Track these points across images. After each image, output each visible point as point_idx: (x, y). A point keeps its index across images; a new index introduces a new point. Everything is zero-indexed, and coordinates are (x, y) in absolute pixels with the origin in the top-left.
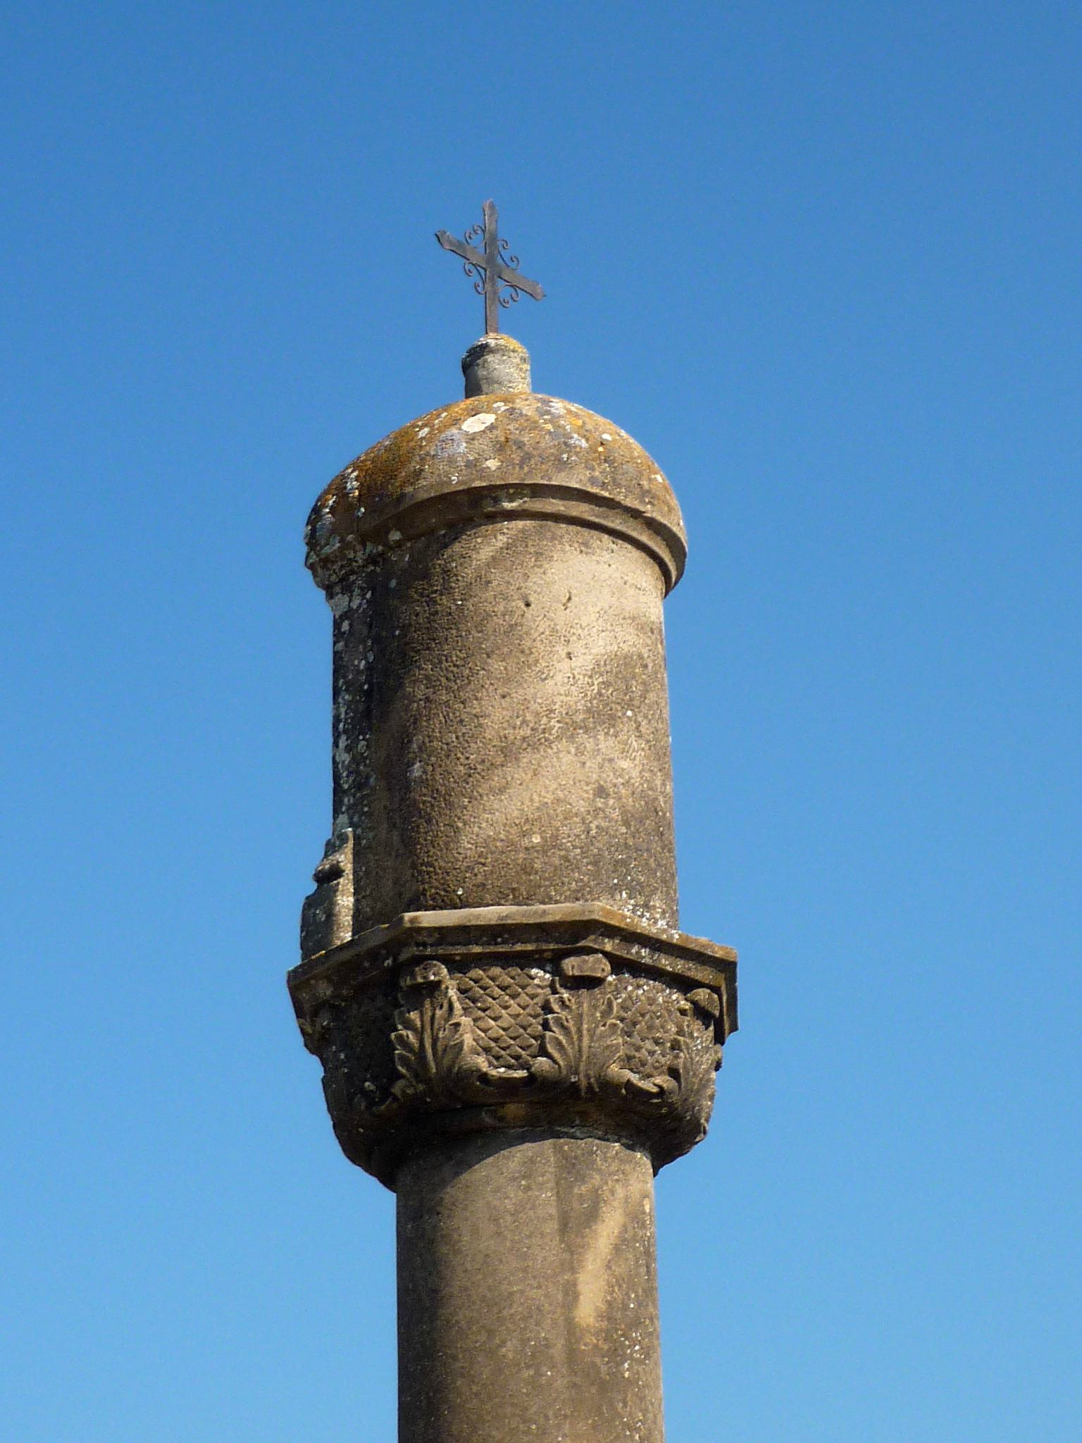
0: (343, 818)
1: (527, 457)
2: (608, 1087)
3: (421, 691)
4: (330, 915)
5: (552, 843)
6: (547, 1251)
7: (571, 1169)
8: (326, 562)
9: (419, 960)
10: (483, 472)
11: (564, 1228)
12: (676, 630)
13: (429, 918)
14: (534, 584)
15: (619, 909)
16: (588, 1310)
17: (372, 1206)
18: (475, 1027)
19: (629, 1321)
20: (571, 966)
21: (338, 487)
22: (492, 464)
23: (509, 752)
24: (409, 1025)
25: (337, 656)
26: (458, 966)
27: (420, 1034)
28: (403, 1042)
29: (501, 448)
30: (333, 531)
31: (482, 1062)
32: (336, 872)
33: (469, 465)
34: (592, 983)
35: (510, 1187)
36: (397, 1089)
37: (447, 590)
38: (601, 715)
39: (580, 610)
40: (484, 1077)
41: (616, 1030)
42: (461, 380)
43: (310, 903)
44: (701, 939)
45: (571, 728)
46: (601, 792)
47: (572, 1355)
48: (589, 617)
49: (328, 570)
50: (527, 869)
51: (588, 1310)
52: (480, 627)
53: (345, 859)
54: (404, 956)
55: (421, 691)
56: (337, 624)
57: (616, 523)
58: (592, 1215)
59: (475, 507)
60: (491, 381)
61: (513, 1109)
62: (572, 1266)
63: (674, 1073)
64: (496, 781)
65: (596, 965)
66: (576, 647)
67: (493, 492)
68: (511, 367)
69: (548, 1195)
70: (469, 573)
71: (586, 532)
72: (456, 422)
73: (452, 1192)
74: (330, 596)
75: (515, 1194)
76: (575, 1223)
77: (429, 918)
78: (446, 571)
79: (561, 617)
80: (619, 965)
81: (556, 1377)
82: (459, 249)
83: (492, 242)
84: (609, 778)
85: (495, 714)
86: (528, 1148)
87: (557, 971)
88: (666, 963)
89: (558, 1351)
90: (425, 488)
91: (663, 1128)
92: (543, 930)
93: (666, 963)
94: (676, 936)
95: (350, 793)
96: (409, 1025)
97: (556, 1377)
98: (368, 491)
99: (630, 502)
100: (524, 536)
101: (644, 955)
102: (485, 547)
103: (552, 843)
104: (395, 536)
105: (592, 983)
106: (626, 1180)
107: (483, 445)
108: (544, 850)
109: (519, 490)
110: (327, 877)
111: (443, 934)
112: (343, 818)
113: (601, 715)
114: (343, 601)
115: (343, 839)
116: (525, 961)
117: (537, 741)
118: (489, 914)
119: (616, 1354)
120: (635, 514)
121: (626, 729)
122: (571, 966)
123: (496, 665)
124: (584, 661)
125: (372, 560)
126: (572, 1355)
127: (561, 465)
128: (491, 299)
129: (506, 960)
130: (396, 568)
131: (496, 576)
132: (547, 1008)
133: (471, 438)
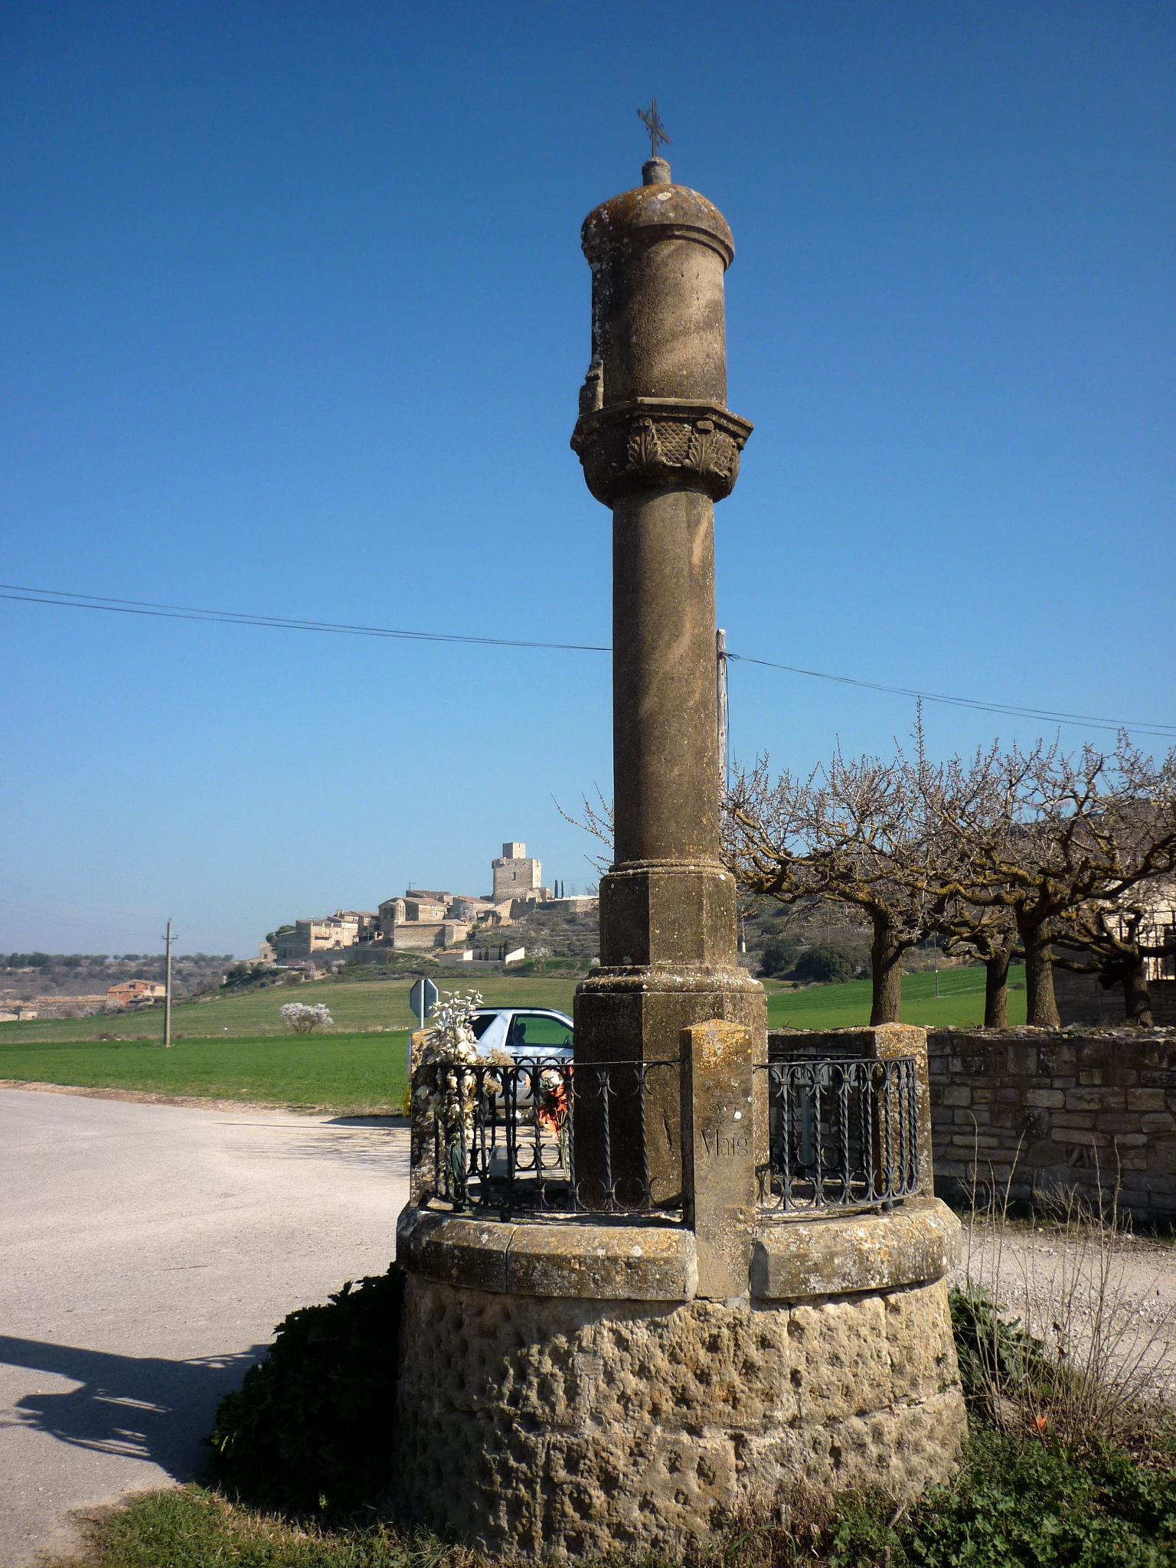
0: (597, 356)
1: (685, 214)
2: (709, 472)
3: (636, 307)
4: (594, 395)
5: (690, 375)
6: (682, 534)
7: (692, 504)
8: (592, 248)
9: (640, 417)
10: (668, 218)
11: (689, 527)
12: (729, 289)
13: (648, 400)
14: (686, 266)
15: (713, 402)
16: (696, 559)
17: (603, 516)
18: (663, 445)
19: (707, 563)
20: (700, 424)
21: (596, 215)
22: (672, 215)
23: (674, 336)
24: (635, 442)
25: (594, 289)
26: (656, 420)
27: (640, 446)
28: (633, 449)
29: (675, 208)
30: (596, 234)
31: (664, 459)
32: (597, 377)
33: (662, 214)
34: (707, 432)
35: (668, 510)
36: (628, 467)
37: (649, 265)
38: (708, 325)
39: (702, 278)
40: (664, 465)
41: (710, 451)
42: (641, 177)
43: (583, 389)
44: (744, 419)
45: (699, 328)
46: (708, 356)
47: (691, 574)
48: (705, 284)
49: (591, 251)
50: (681, 384)
51: (696, 559)
52: (664, 282)
53: (600, 372)
54: (636, 414)
55: (636, 307)
56: (594, 275)
57: (715, 245)
58: (698, 523)
59: (664, 232)
60: (657, 177)
61: (672, 479)
62: (691, 541)
63: (730, 470)
64: (668, 347)
65: (709, 425)
66: (700, 295)
67: (671, 227)
68: (664, 173)
69: (683, 513)
70: (659, 259)
71: (705, 248)
72: (654, 195)
73: (644, 509)
74: (591, 261)
75: (670, 512)
76: (692, 525)
77: (648, 400)
78: (648, 258)
79: (695, 282)
80: (718, 426)
81: (685, 582)
82: (645, 119)
83: (655, 117)
84: (711, 350)
85: (669, 319)
86: (676, 494)
87: (694, 426)
88: (731, 427)
89: (686, 573)
90: (643, 221)
91: (718, 487)
92: (691, 409)
93: (731, 427)
94: (736, 416)
95: (598, 345)
96: (635, 442)
97: (685, 582)
98: (613, 220)
99: (721, 237)
100: (681, 247)
101: (724, 422)
102: (667, 249)
103: (690, 375)
104: (626, 240)
105: (707, 432)
106: (710, 511)
107: (667, 206)
108: (688, 377)
109: (681, 227)
110: (591, 380)
111: (652, 407)
112: (597, 356)
113: (708, 325)
114: (597, 265)
115: (599, 364)
116: (682, 421)
117: (686, 332)
118: (672, 401)
119: (705, 575)
120: (722, 242)
121: (716, 331)
122: (700, 424)
123: (669, 299)
124: (703, 302)
125: (613, 249)
126: (691, 574)
127: (699, 218)
128: (654, 143)
129: (675, 420)
130: (624, 258)
131: (670, 262)
132: (690, 440)
133: (662, 202)
